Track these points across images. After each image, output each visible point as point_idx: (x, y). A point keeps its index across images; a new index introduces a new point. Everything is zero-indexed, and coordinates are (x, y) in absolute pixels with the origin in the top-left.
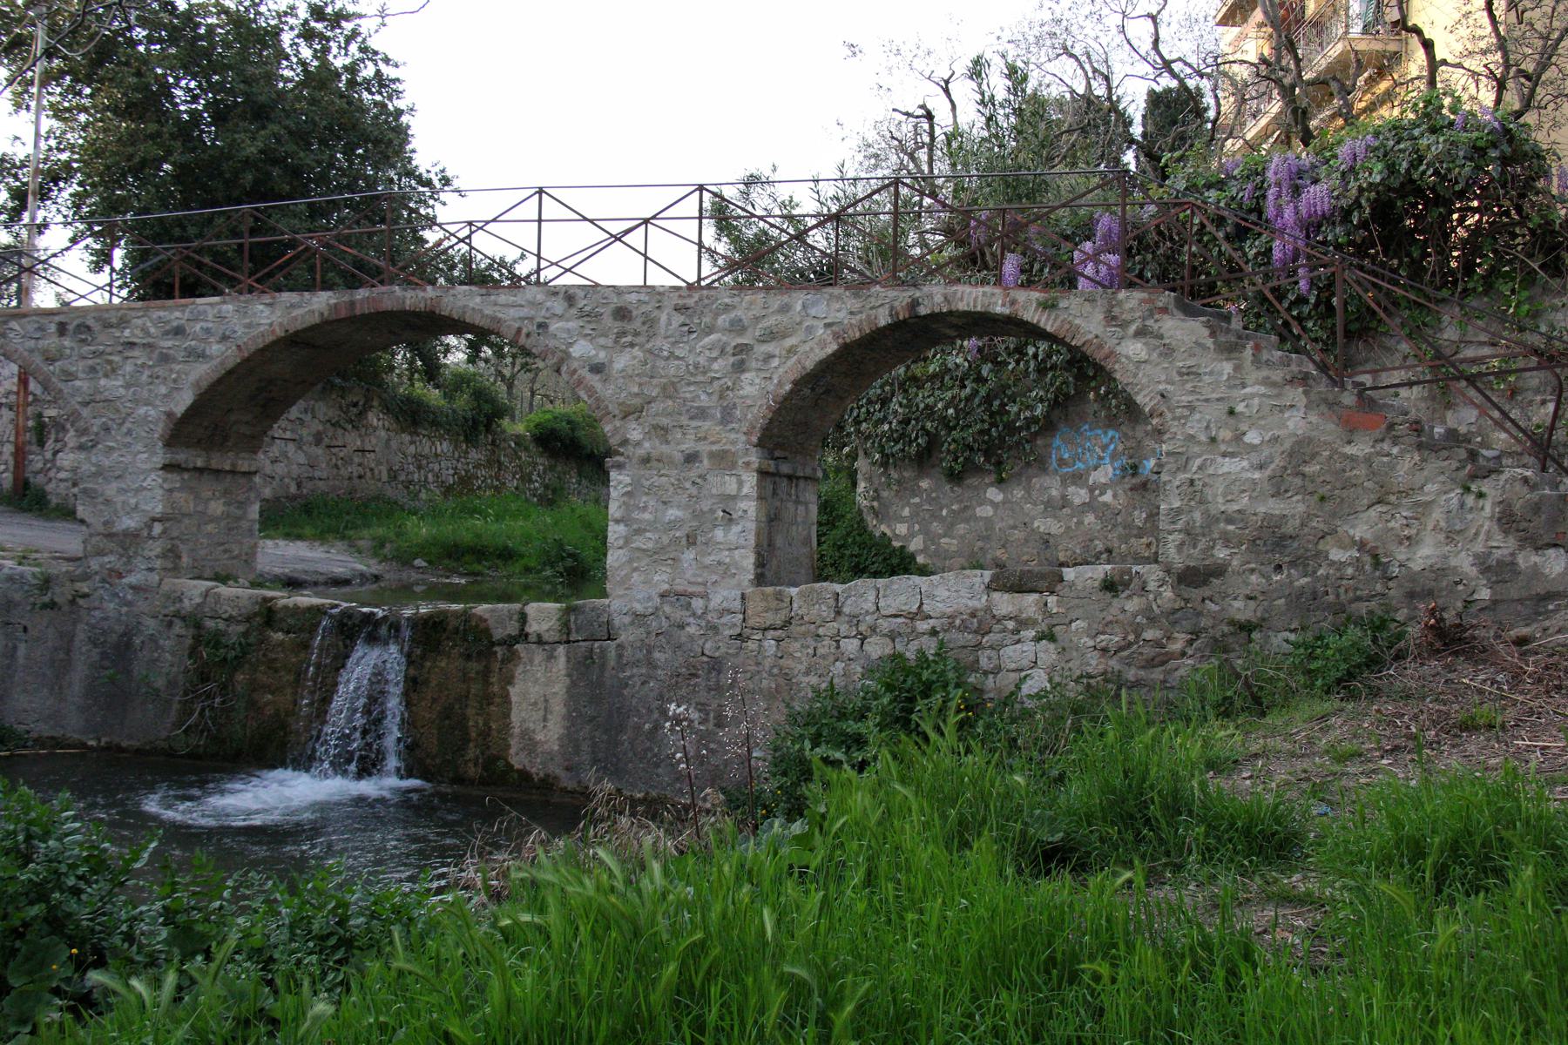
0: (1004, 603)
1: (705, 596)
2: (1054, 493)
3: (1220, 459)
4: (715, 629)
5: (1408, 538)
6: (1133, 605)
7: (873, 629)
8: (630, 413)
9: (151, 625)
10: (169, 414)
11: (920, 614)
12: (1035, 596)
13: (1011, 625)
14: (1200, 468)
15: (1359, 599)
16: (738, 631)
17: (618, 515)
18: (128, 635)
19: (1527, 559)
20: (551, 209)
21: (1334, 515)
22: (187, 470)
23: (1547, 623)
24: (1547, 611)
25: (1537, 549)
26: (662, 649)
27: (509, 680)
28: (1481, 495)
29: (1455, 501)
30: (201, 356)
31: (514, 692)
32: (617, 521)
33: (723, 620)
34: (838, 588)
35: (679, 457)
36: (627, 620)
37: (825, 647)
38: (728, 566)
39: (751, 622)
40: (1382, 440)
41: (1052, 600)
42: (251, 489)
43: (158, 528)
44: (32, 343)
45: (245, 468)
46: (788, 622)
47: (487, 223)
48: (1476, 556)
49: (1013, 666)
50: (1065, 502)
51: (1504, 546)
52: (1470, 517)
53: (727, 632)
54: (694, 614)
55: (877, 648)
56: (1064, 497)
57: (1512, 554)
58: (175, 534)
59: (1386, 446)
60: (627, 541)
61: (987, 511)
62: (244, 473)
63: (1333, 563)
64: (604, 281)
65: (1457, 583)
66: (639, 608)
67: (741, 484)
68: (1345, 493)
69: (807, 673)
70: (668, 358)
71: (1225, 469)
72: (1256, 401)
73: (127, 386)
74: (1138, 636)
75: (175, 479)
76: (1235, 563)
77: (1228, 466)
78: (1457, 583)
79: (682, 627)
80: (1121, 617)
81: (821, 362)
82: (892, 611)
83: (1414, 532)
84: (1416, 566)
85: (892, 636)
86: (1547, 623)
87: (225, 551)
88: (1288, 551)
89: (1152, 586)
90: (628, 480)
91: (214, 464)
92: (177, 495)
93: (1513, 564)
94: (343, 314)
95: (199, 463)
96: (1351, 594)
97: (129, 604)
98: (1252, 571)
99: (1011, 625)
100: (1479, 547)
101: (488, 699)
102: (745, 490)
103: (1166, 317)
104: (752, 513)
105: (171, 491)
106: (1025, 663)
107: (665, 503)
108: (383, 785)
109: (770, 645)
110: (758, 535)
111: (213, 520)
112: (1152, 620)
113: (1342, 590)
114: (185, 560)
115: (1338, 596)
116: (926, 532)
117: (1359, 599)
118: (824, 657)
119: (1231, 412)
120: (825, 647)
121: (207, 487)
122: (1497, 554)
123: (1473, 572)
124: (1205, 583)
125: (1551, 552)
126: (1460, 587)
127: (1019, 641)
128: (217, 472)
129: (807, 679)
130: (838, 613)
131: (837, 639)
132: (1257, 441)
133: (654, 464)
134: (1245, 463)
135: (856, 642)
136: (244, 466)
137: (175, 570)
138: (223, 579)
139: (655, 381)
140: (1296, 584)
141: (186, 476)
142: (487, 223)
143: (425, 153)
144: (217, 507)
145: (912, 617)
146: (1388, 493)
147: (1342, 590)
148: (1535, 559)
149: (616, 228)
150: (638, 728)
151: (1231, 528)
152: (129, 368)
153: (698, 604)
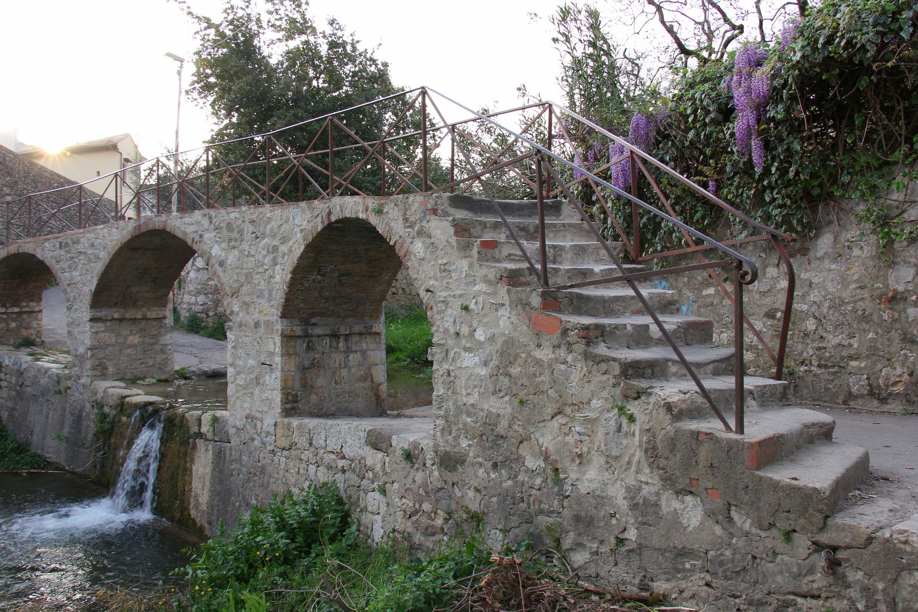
5: (580, 456)
8: (235, 293)
9: (88, 405)
18: (81, 411)
19: (670, 503)
21: (529, 421)
22: (106, 320)
23: (683, 584)
24: (684, 570)
25: (678, 493)
27: (192, 461)
28: (632, 419)
29: (613, 423)
31: (194, 468)
35: (252, 323)
40: (559, 346)
42: (162, 327)
44: (51, 253)
45: (154, 315)
48: (628, 490)
51: (650, 482)
52: (625, 442)
55: (323, 476)
57: (658, 494)
58: (101, 356)
59: (562, 352)
62: (155, 319)
63: (527, 470)
65: (612, 516)
68: (535, 399)
70: (247, 256)
72: (481, 299)
75: (100, 326)
76: (471, 454)
78: (612, 516)
80: (412, 486)
83: (585, 449)
84: (583, 488)
86: (683, 584)
87: (142, 364)
91: (127, 316)
92: (101, 335)
93: (656, 505)
95: (116, 316)
98: (481, 464)
100: (631, 481)
101: (186, 469)
103: (433, 217)
105: (97, 333)
107: (248, 355)
108: (144, 515)
114: (111, 369)
119: (466, 308)
121: (125, 330)
122: (646, 490)
123: (623, 504)
125: (689, 499)
126: (614, 521)
128: (134, 320)
130: (311, 444)
133: (243, 327)
134: (477, 359)
136: (152, 314)
137: (104, 376)
138: (133, 381)
139: (243, 271)
141: (108, 324)
143: (401, 78)
144: (134, 339)
146: (565, 404)
148: (676, 504)
150: (234, 504)
151: (469, 420)
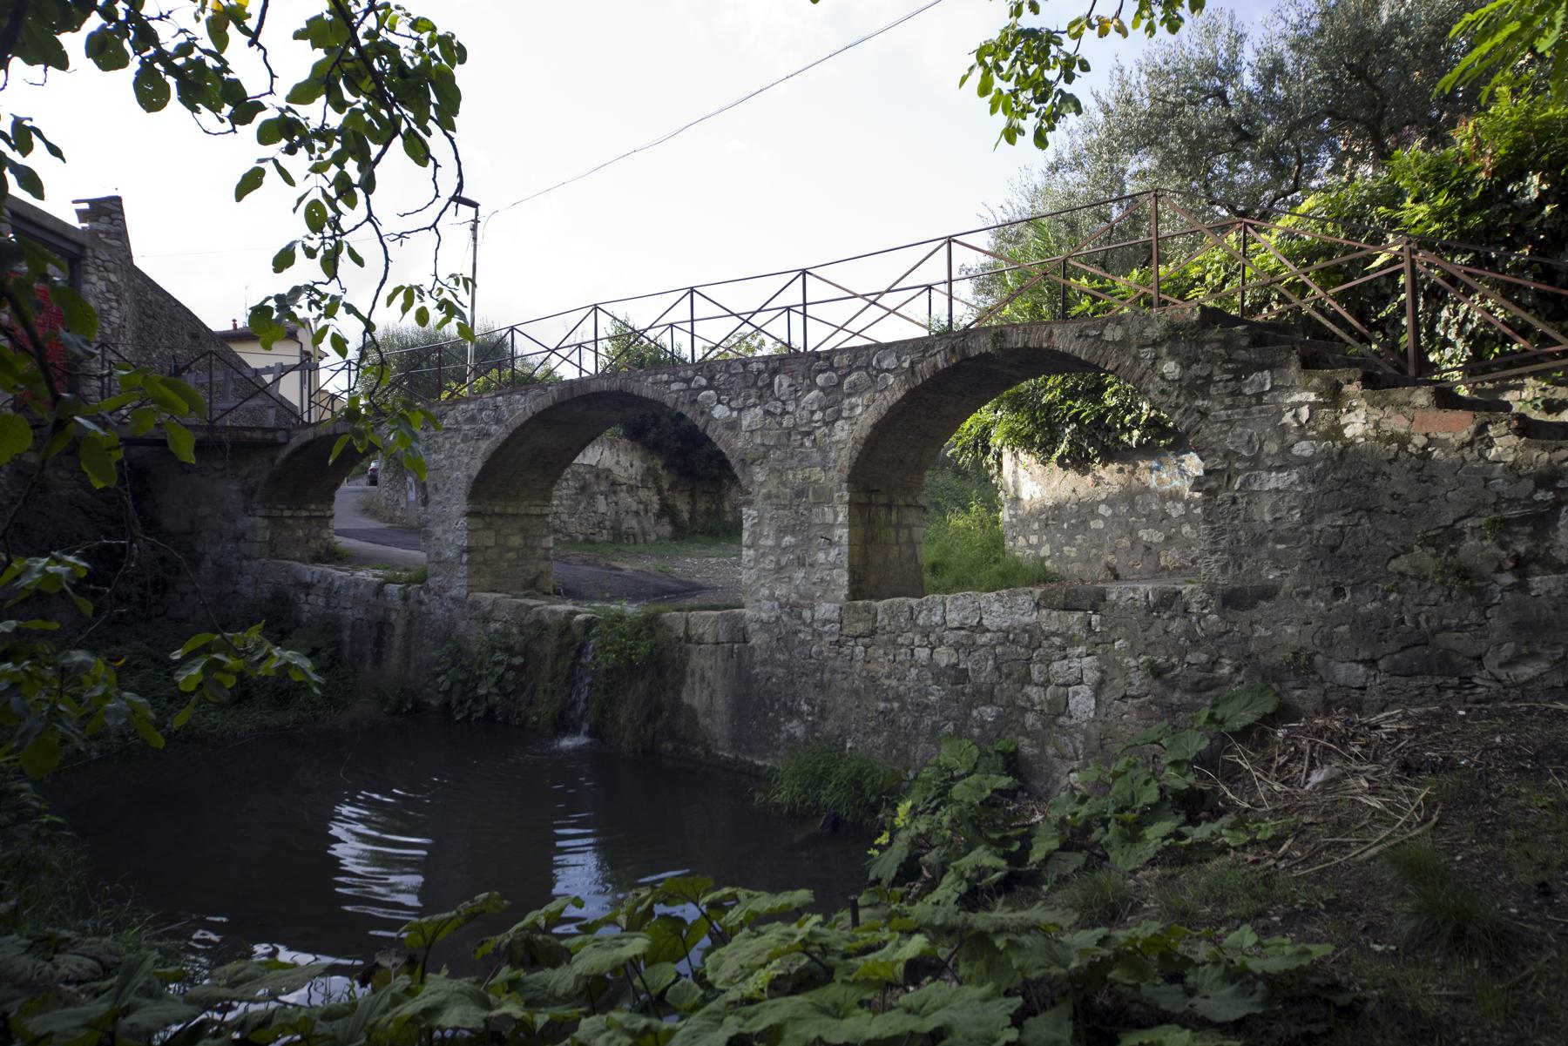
0: (1052, 621)
1: (812, 608)
2: (1155, 507)
3: (1264, 475)
4: (820, 635)
6: (1177, 626)
7: (941, 640)
10: (470, 477)
11: (980, 628)
12: (1080, 614)
13: (1057, 641)
14: (1242, 485)
15: (1447, 629)
16: (836, 638)
17: (749, 542)
20: (816, 290)
26: (781, 651)
30: (488, 435)
32: (749, 547)
33: (827, 628)
34: (914, 602)
36: (757, 626)
37: (903, 655)
38: (829, 583)
39: (845, 631)
41: (1095, 618)
43: (465, 558)
46: (873, 633)
47: (881, 294)
49: (1061, 681)
50: (1167, 516)
53: (827, 639)
54: (804, 623)
56: (1163, 511)
60: (757, 561)
61: (1099, 524)
64: (884, 340)
66: (764, 616)
67: (836, 515)
69: (888, 677)
71: (1272, 485)
73: (447, 458)
74: (1182, 660)
75: (479, 523)
77: (1275, 480)
79: (796, 633)
81: (891, 409)
82: (956, 624)
85: (957, 646)
88: (1351, 571)
89: (1194, 608)
90: (755, 513)
91: (510, 510)
94: (567, 397)
96: (1434, 623)
97: (450, 610)
99: (1057, 641)
102: (840, 519)
104: (845, 540)
106: (1071, 679)
109: (859, 649)
110: (851, 556)
111: (512, 550)
112: (1196, 643)
113: (1422, 619)
115: (1418, 625)
116: (1051, 541)
117: (1447, 629)
118: (901, 663)
120: (903, 655)
124: (1253, 606)
127: (1065, 657)
129: (887, 682)
131: (911, 647)
132: (1308, 453)
135: (927, 651)
140: (1361, 610)
142: (881, 294)
145: (973, 629)
147: (1422, 619)
149: (872, 298)
152: (448, 446)
153: (807, 614)
